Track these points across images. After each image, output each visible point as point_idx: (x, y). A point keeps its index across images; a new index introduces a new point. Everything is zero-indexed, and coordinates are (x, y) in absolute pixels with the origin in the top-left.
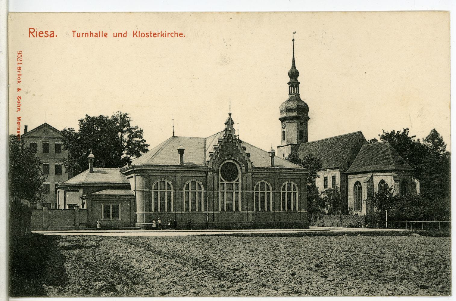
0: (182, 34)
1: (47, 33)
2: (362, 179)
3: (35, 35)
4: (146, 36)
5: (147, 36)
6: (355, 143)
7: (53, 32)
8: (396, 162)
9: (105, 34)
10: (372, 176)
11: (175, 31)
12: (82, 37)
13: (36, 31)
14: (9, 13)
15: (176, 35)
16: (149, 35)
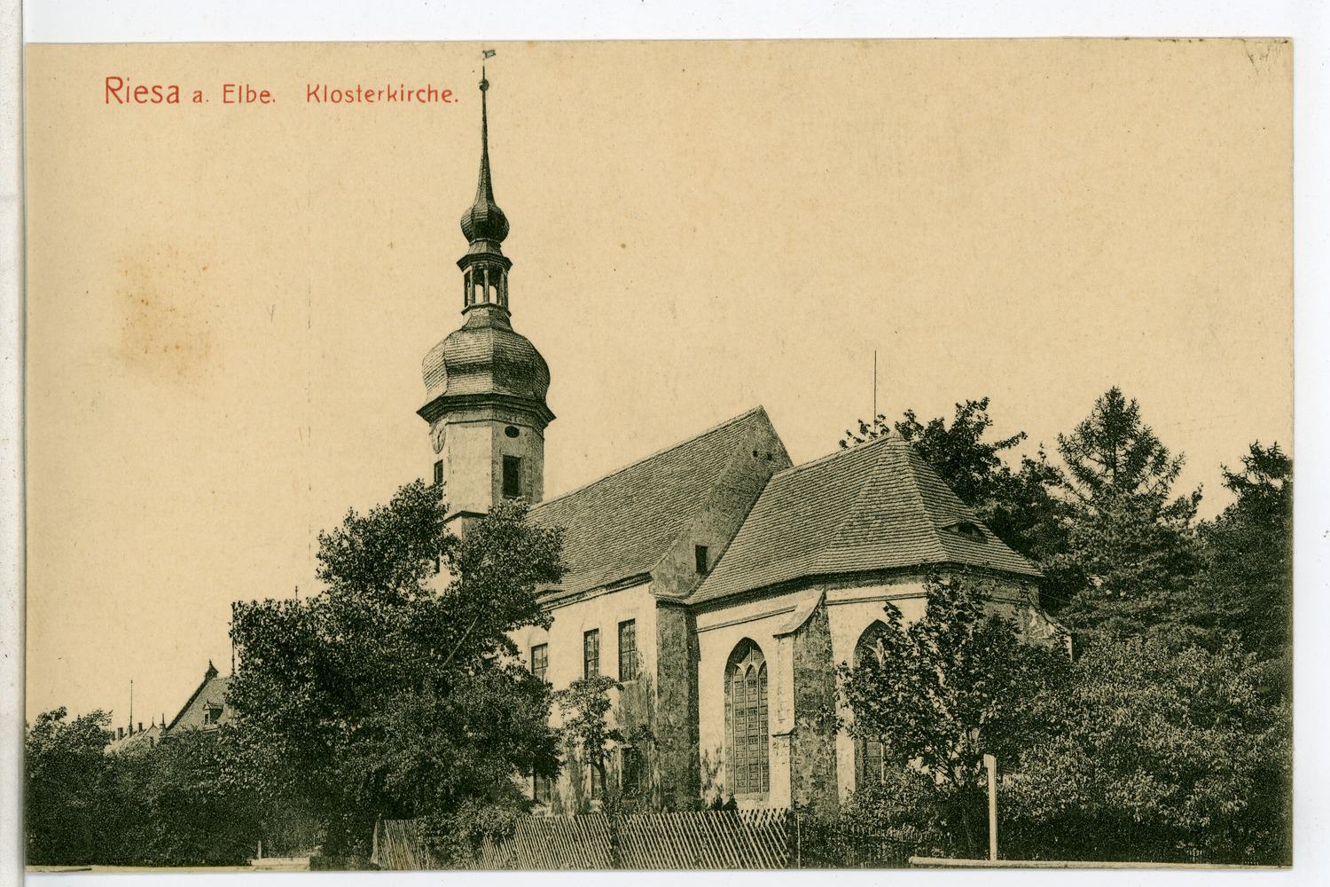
0: (268, 95)
1: (157, 89)
2: (765, 623)
3: (124, 98)
5: (350, 99)
6: (744, 467)
8: (946, 528)
10: (823, 603)
11: (429, 86)
12: (409, 99)
15: (433, 95)
16: (355, 95)
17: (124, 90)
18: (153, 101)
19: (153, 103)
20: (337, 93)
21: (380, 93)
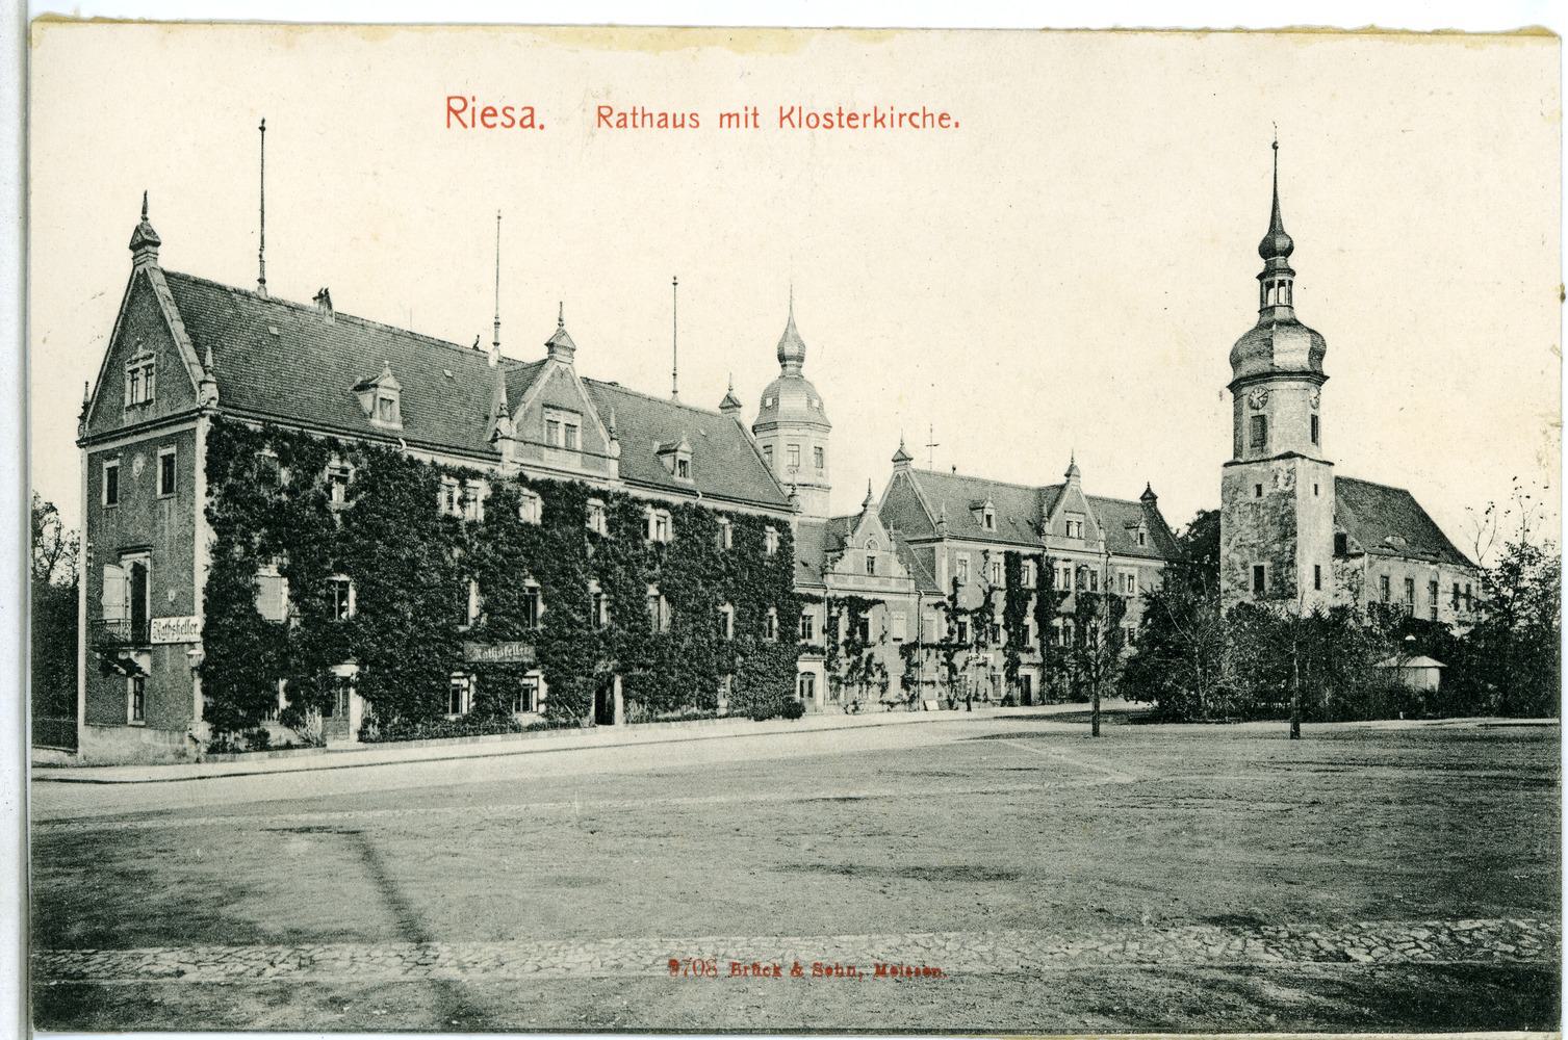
1: (508, 112)
3: (469, 122)
4: (825, 126)
5: (829, 124)
7: (532, 109)
9: (490, 112)
13: (470, 105)
14: (36, 30)
15: (928, 119)
16: (835, 119)
17: (469, 111)
21: (865, 116)
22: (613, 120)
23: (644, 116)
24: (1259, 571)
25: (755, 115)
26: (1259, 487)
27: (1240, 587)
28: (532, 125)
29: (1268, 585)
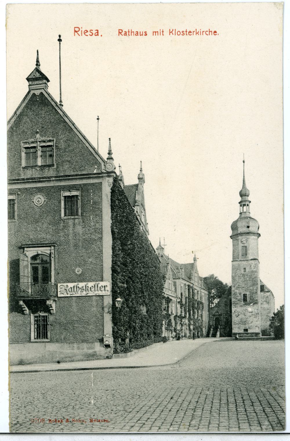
1: (91, 31)
3: (80, 35)
4: (182, 35)
5: (183, 34)
13: (81, 29)
16: (185, 33)
17: (80, 31)
18: (90, 35)
19: (182, 36)
20: (179, 32)
22: (123, 33)
23: (131, 32)
24: (245, 296)
25: (163, 32)
26: (245, 269)
27: (239, 300)
28: (98, 35)
29: (248, 300)
